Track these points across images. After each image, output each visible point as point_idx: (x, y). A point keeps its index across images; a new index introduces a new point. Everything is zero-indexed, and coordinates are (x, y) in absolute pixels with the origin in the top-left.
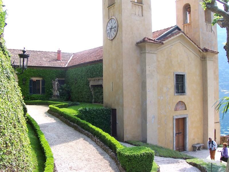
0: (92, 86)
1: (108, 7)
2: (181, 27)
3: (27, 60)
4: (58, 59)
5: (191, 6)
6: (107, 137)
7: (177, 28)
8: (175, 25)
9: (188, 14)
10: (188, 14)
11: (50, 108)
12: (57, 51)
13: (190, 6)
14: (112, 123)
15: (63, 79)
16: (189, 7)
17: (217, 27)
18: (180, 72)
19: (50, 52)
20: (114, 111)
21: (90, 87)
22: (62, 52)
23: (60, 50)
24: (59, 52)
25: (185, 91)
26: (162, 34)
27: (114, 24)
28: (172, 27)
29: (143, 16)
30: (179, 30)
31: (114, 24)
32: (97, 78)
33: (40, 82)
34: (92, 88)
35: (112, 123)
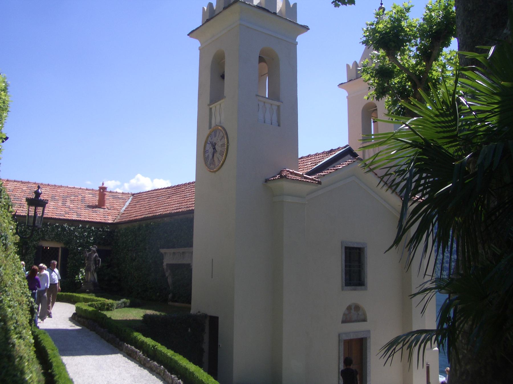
0: (167, 265)
1: (208, 105)
2: (356, 150)
3: (29, 213)
4: (101, 204)
5: (378, 108)
6: (197, 374)
7: (349, 152)
8: (345, 145)
9: (372, 123)
10: (372, 123)
11: (77, 309)
12: (98, 189)
13: (376, 107)
14: (372, 121)
15: (108, 248)
16: (374, 110)
17: (404, 182)
18: (354, 240)
19: (83, 189)
20: (214, 321)
21: (165, 267)
22: (108, 190)
23: (105, 186)
24: (103, 189)
25: (364, 281)
26: (319, 162)
27: (221, 140)
28: (338, 149)
29: (279, 125)
30: (354, 155)
31: (221, 140)
32: (181, 250)
33: (58, 252)
34: (169, 271)
35: (372, 121)
